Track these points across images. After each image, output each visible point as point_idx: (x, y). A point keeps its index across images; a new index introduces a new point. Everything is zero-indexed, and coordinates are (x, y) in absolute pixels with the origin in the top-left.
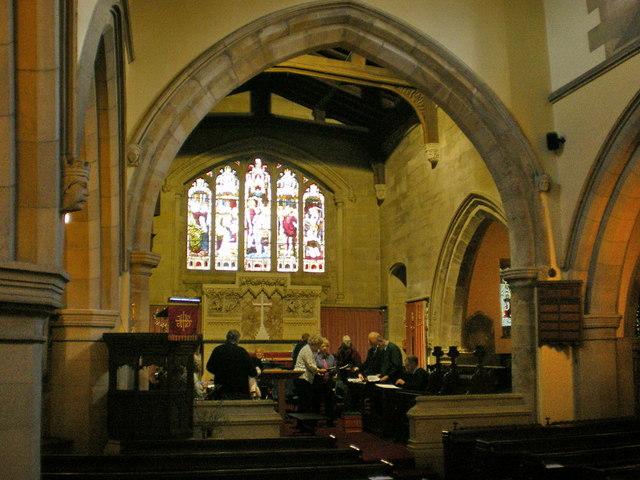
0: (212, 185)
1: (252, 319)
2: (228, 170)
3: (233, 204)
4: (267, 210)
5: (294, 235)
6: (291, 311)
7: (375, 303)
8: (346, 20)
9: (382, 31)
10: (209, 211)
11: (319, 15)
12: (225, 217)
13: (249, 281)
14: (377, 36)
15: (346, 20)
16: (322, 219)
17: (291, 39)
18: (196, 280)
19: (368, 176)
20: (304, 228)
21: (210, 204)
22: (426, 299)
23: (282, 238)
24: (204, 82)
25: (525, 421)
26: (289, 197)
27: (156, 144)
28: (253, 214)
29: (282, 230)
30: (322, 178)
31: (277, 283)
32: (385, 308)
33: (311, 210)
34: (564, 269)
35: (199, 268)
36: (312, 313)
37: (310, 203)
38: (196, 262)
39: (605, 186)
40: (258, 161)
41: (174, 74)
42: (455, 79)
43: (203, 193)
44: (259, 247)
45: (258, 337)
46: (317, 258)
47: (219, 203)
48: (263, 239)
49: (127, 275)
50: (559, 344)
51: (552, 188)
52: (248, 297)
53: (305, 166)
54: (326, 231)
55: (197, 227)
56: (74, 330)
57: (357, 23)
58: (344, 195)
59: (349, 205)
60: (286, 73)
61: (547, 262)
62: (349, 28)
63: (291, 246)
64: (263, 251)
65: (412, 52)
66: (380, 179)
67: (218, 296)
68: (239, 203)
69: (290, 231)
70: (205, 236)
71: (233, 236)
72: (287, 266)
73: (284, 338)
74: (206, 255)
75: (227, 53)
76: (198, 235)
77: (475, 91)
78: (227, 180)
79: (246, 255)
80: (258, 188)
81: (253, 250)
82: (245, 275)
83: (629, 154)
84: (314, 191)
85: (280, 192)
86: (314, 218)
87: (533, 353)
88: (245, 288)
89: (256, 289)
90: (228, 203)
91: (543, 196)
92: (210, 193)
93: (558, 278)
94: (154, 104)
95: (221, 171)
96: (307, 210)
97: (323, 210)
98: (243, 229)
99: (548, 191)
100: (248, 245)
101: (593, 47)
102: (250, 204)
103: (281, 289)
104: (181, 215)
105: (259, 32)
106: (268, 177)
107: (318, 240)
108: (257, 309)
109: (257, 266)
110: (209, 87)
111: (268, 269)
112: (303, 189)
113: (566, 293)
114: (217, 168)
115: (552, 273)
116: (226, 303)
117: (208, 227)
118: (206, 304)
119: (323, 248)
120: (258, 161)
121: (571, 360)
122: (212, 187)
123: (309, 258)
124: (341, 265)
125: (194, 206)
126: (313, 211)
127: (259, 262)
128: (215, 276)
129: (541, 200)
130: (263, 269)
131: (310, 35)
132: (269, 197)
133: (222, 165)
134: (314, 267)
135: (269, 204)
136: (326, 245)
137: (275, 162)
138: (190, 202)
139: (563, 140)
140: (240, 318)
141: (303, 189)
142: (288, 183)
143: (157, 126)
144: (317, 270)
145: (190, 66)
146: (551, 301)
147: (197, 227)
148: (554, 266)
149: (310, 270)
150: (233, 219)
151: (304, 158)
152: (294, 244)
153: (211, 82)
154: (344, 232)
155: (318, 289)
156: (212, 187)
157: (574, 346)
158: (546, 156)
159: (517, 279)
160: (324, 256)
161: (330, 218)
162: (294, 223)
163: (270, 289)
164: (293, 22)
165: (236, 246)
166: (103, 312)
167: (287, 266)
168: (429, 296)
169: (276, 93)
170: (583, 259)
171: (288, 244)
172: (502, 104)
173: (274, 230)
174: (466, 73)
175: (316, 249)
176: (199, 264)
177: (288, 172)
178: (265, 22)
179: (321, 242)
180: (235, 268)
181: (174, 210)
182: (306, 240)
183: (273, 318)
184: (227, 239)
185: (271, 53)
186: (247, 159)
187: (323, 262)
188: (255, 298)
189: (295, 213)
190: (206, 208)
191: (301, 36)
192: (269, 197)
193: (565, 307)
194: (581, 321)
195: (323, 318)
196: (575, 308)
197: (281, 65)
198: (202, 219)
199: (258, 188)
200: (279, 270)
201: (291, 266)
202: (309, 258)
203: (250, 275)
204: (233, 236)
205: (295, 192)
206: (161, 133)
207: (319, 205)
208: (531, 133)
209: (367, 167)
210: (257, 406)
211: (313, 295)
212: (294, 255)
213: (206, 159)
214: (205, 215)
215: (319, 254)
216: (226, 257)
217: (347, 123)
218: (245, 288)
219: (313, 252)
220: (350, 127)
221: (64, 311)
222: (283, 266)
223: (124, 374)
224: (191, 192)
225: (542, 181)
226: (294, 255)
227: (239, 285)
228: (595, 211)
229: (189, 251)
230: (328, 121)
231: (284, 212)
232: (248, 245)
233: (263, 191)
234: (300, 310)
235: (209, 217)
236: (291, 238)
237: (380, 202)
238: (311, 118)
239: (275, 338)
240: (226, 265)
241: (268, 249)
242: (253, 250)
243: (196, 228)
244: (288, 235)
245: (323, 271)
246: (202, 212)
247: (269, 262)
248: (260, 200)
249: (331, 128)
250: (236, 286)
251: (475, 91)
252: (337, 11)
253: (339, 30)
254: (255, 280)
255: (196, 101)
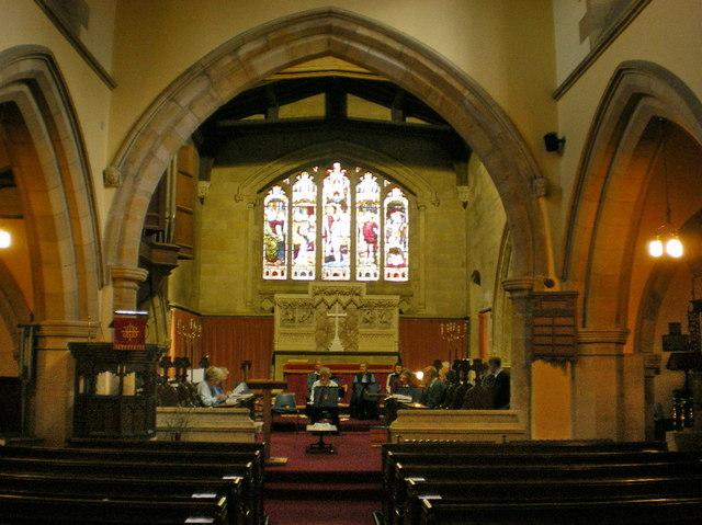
0: (288, 191)
1: (327, 330)
2: (305, 175)
3: (310, 211)
4: (347, 217)
5: (375, 242)
6: (368, 321)
7: (459, 314)
8: (329, 30)
9: (367, 38)
10: (286, 219)
11: (299, 28)
12: (302, 225)
13: (323, 291)
14: (363, 44)
15: (329, 30)
16: (405, 225)
17: (269, 55)
18: (269, 290)
19: (451, 177)
20: (385, 234)
21: (287, 211)
22: (490, 310)
23: (362, 245)
24: (184, 102)
25: (524, 438)
26: (370, 203)
27: (137, 164)
28: (331, 221)
29: (362, 237)
30: (403, 181)
31: (353, 292)
32: (468, 318)
33: (393, 215)
34: (563, 278)
35: (274, 278)
36: (390, 324)
37: (392, 208)
38: (272, 271)
39: (591, 191)
40: (337, 166)
41: (152, 99)
42: (445, 81)
43: (279, 201)
44: (337, 256)
45: (332, 349)
46: (399, 266)
47: (296, 212)
48: (342, 247)
49: (110, 289)
50: (553, 359)
51: (551, 192)
52: (322, 307)
53: (383, 169)
54: (410, 236)
55: (274, 236)
56: (53, 340)
57: (341, 32)
58: (426, 196)
59: (432, 209)
60: (332, 77)
61: (546, 272)
62: (333, 38)
63: (372, 254)
64: (342, 259)
65: (400, 56)
66: (463, 180)
67: (290, 306)
68: (315, 210)
69: (370, 238)
70: (281, 245)
71: (310, 244)
72: (368, 275)
73: (360, 349)
74: (283, 264)
75: (205, 73)
76: (274, 244)
77: (466, 93)
78: (304, 185)
79: (323, 264)
80: (337, 193)
81: (331, 259)
82: (355, 285)
83: (611, 155)
84: (396, 195)
85: (359, 198)
86: (397, 225)
87: (528, 367)
88: (318, 298)
89: (330, 299)
90: (305, 211)
91: (542, 202)
92: (286, 201)
93: (556, 288)
94: (134, 127)
95: (298, 177)
96: (388, 215)
97: (407, 215)
98: (320, 236)
99: (547, 195)
100: (326, 253)
101: (582, 39)
102: (328, 210)
103: (356, 299)
104: (256, 224)
105: (236, 50)
106: (348, 182)
107: (401, 247)
108: (331, 320)
109: (335, 275)
110: (191, 107)
111: (348, 277)
112: (385, 193)
113: (561, 305)
114: (293, 173)
115: (550, 284)
116: (299, 314)
117: (284, 236)
118: (278, 314)
119: (406, 255)
120: (337, 166)
121: (569, 377)
122: (289, 194)
123: (391, 266)
124: (422, 274)
125: (271, 214)
126: (396, 216)
127: (338, 270)
128: (291, 285)
129: (538, 205)
130: (341, 278)
131: (292, 48)
132: (349, 203)
133: (299, 171)
134: (396, 275)
135: (349, 210)
136: (409, 252)
137: (355, 164)
138: (266, 211)
139: (563, 141)
140: (313, 329)
141: (385, 193)
142: (369, 186)
143: (137, 148)
144: (400, 279)
145: (167, 90)
146: (543, 314)
147: (274, 236)
148: (552, 276)
149: (392, 279)
150: (310, 227)
151: (385, 162)
152: (375, 251)
153: (192, 102)
154: (426, 237)
155: (396, 299)
156: (289, 194)
157: (573, 363)
158: (547, 159)
159: (517, 290)
160: (407, 263)
161: (413, 222)
162: (375, 229)
163: (344, 299)
164: (272, 36)
165: (313, 254)
166: (78, 323)
167: (368, 275)
168: (491, 306)
169: (354, 94)
170: (578, 268)
171: (368, 251)
172: (496, 104)
173: (353, 237)
174: (456, 75)
175: (399, 256)
176: (275, 274)
177: (368, 176)
178: (243, 40)
179: (405, 249)
180: (313, 278)
181: (247, 219)
182: (387, 248)
183: (348, 329)
184: (304, 247)
185: (252, 69)
186: (324, 165)
187: (406, 270)
188: (329, 308)
189: (376, 219)
190: (283, 216)
191: (281, 50)
192: (349, 203)
193: (559, 321)
194: (575, 335)
195: (401, 329)
196: (570, 321)
197: (285, 71)
198: (278, 227)
199: (337, 193)
200: (358, 278)
201: (372, 275)
202: (391, 266)
203: (328, 285)
204: (310, 244)
205: (376, 197)
206: (142, 155)
207: (402, 210)
208: (525, 128)
209: (449, 167)
210: (234, 414)
211: (388, 305)
212: (375, 263)
213: (279, 167)
214: (282, 223)
215: (402, 262)
216: (303, 266)
217: (401, 125)
218: (318, 298)
219: (396, 260)
220: (435, 126)
221: (43, 323)
222: (271, 274)
223: (105, 383)
224: (267, 200)
225: (539, 183)
226: (375, 263)
227: (320, 294)
228: (588, 210)
229: (265, 261)
230: (409, 120)
231: (364, 218)
232: (326, 253)
233: (342, 197)
234: (377, 321)
235: (286, 225)
236: (371, 246)
237: (465, 205)
238: (390, 119)
239: (351, 350)
240: (303, 274)
241: (347, 257)
242: (331, 259)
243: (273, 236)
244: (368, 242)
245: (406, 279)
246: (279, 220)
247: (348, 270)
248: (338, 206)
249: (413, 128)
250: (308, 297)
251: (466, 93)
252: (317, 21)
253: (322, 40)
254: (335, 289)
255: (177, 121)
